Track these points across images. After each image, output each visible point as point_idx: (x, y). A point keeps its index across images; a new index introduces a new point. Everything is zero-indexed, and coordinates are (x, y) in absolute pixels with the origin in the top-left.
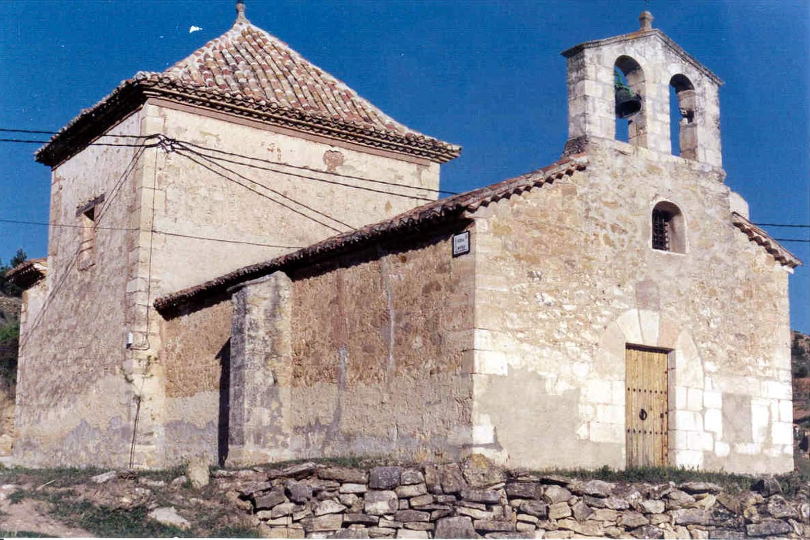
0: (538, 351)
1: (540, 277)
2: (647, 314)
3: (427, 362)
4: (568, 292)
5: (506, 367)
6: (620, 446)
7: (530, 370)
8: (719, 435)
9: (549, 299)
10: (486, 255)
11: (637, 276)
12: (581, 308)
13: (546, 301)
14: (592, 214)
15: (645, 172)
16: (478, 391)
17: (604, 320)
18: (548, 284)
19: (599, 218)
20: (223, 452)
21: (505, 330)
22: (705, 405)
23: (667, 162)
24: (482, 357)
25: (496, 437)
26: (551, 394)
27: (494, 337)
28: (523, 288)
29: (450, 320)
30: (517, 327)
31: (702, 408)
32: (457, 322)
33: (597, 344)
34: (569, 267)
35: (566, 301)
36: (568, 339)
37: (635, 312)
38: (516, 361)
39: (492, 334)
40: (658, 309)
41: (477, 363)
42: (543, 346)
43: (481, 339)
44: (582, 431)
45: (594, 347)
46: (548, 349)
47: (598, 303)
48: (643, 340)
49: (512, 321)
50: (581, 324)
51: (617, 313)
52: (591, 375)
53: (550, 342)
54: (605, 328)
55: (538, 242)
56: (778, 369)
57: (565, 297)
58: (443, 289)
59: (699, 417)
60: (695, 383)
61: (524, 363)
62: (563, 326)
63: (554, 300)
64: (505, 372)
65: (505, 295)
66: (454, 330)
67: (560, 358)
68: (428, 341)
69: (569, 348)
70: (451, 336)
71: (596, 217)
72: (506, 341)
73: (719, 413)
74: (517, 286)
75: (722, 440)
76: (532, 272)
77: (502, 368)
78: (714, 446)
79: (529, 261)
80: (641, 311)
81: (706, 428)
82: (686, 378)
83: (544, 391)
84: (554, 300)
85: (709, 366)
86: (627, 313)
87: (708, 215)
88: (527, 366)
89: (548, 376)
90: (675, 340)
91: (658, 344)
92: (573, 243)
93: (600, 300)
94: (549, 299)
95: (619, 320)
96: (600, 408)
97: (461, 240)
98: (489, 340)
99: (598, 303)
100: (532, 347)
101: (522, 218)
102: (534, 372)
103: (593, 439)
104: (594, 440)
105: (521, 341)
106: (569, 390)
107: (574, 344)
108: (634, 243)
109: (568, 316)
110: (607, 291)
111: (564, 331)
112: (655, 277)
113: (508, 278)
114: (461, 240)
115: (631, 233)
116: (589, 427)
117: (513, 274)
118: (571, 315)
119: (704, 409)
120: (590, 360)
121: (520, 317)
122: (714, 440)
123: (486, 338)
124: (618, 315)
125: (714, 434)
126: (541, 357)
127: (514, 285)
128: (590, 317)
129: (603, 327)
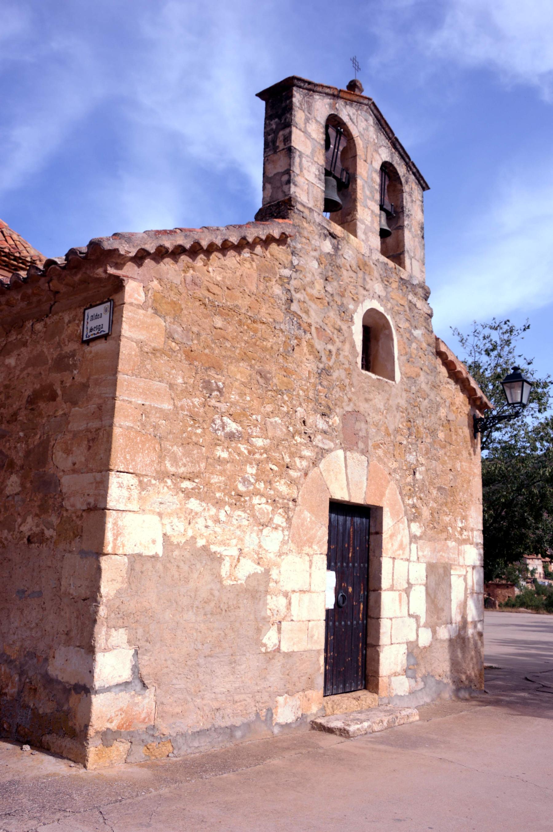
0: (213, 511)
1: (219, 390)
2: (355, 457)
3: (24, 521)
4: (259, 418)
5: (160, 540)
6: (318, 651)
7: (201, 542)
8: (423, 621)
9: (232, 426)
10: (140, 344)
11: (344, 404)
12: (277, 444)
13: (228, 429)
14: (294, 307)
15: (355, 267)
16: (108, 587)
17: (305, 463)
18: (233, 404)
19: (303, 315)
20: (16, 494)
21: (162, 476)
22: (411, 581)
23: (378, 260)
24: (120, 523)
25: (136, 670)
26: (228, 582)
27: (142, 486)
28: (194, 406)
29: (68, 451)
30: (182, 470)
31: (407, 586)
32: (80, 454)
33: (294, 500)
34: (261, 381)
35: (256, 431)
36: (257, 493)
37: (340, 453)
38: (178, 529)
39: (140, 482)
40: (365, 452)
41: (109, 536)
42: (219, 504)
43: (119, 490)
44: (270, 638)
45: (291, 504)
46: (227, 508)
47: (297, 438)
48: (350, 496)
49: (175, 461)
50: (275, 468)
51: (322, 453)
52: (285, 548)
53: (231, 496)
54: (306, 474)
55: (220, 337)
56: (472, 530)
57: (256, 426)
58: (59, 399)
59: (404, 595)
60: (401, 552)
61: (190, 533)
62: (251, 470)
63: (240, 429)
64: (158, 549)
65: (166, 416)
66: (74, 471)
67: (245, 523)
68: (28, 485)
69: (257, 507)
70: (67, 482)
71: (299, 313)
72: (165, 495)
73: (423, 588)
74: (184, 402)
75: (424, 626)
76: (209, 382)
77: (154, 542)
78: (418, 636)
79: (203, 365)
80: (348, 453)
81: (411, 612)
82: (392, 545)
83: (219, 578)
84: (240, 429)
85: (416, 529)
86: (333, 454)
87: (415, 337)
88: (193, 538)
89: (224, 553)
90: (382, 495)
91: (365, 499)
92: (269, 345)
93: (300, 434)
94: (232, 426)
95: (322, 465)
96: (295, 598)
97: (97, 316)
98: (135, 493)
99: (297, 438)
100: (204, 504)
101: (201, 293)
102: (205, 548)
103: (284, 648)
104: (286, 651)
105: (188, 494)
106: (255, 574)
107: (264, 500)
108: (341, 358)
109: (257, 456)
110: (309, 421)
111: (253, 481)
112: (363, 407)
113: (171, 386)
114: (97, 316)
115: (338, 344)
116: (279, 630)
117: (180, 381)
118: (261, 454)
119: (410, 585)
120: (284, 525)
121: (188, 454)
122: (418, 627)
123: (129, 488)
124: (323, 456)
125: (417, 618)
126: (217, 521)
127: (180, 400)
128: (287, 460)
129: (303, 474)
